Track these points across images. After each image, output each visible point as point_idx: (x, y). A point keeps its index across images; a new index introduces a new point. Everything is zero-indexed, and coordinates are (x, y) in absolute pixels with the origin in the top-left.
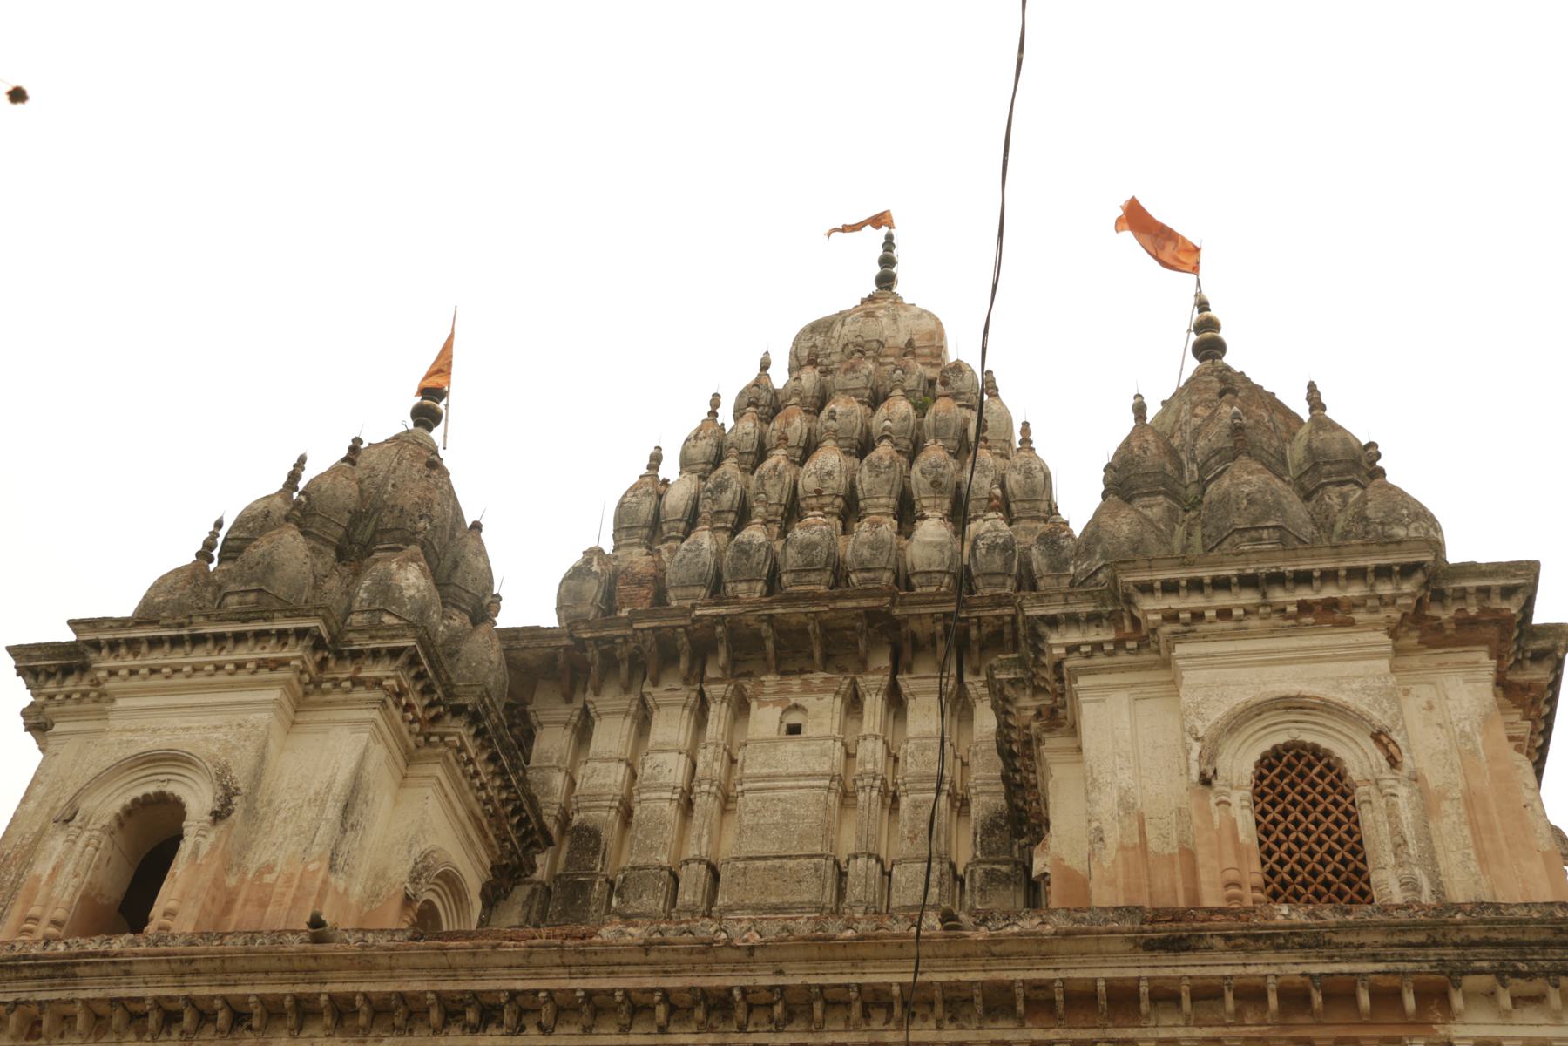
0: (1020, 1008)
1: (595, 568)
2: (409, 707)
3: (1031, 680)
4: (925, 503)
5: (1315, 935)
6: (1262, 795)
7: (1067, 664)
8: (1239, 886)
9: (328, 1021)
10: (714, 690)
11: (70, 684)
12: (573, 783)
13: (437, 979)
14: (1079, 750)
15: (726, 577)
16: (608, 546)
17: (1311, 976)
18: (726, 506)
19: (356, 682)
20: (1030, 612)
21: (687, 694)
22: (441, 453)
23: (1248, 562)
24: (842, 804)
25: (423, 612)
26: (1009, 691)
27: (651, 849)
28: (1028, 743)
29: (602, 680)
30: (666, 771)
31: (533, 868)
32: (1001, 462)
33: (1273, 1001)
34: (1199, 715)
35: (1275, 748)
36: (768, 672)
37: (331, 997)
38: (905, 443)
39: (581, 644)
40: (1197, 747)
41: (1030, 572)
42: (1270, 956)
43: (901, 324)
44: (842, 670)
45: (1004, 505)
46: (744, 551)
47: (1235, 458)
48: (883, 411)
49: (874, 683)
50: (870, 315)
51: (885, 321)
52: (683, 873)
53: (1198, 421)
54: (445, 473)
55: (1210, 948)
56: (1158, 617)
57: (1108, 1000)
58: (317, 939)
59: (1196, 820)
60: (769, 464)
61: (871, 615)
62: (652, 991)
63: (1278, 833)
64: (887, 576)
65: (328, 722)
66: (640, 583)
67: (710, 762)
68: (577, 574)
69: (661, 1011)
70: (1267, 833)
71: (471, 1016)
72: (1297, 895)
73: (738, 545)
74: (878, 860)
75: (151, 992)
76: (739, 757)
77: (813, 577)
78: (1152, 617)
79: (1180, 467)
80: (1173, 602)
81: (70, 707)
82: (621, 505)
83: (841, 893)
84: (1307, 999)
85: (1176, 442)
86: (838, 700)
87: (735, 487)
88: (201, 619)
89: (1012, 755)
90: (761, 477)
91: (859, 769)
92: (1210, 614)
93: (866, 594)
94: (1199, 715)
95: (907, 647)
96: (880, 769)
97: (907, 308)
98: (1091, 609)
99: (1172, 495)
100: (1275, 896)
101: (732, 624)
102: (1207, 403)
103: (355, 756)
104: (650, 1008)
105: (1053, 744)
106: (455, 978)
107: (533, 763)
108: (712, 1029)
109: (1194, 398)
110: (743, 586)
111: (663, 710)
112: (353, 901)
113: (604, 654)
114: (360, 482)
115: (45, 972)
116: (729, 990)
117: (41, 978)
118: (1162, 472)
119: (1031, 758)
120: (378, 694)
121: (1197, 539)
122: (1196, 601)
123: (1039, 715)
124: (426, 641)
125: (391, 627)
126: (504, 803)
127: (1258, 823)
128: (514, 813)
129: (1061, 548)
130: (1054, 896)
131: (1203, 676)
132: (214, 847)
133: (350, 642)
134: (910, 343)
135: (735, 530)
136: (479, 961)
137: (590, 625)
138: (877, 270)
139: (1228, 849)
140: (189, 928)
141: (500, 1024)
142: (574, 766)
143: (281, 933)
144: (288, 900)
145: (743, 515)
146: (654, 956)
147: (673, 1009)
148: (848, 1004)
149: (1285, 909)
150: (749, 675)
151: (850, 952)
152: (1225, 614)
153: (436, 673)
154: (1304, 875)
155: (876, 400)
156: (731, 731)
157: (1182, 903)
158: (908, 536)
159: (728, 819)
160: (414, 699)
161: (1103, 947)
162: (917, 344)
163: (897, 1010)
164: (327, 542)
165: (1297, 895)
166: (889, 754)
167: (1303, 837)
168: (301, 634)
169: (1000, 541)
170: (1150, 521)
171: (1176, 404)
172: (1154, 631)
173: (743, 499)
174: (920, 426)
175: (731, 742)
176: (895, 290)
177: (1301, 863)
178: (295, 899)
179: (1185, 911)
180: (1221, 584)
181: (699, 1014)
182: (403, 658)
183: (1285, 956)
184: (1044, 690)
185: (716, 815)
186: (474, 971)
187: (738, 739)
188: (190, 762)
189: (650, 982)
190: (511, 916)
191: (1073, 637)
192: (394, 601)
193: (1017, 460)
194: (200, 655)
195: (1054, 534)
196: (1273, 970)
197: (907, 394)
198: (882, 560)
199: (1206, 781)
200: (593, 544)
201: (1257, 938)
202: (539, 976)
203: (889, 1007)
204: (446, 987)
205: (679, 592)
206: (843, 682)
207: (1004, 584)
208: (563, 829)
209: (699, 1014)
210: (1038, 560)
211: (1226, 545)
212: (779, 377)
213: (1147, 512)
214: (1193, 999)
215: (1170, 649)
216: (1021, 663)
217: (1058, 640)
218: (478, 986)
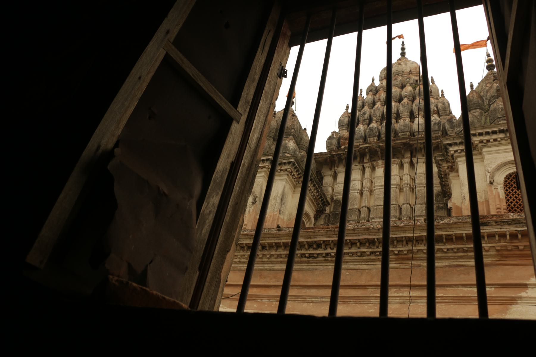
0: (444, 241)
1: (335, 136)
2: (294, 175)
3: (446, 159)
5: (519, 221)
6: (506, 186)
7: (455, 155)
8: (500, 209)
9: (283, 248)
10: (366, 165)
12: (333, 189)
13: (306, 238)
14: (459, 176)
15: (367, 136)
16: (337, 130)
17: (518, 231)
18: (366, 118)
19: (281, 170)
20: (445, 143)
21: (360, 166)
22: (295, 112)
23: (501, 126)
24: (400, 191)
25: (295, 152)
26: (440, 162)
27: (353, 204)
28: (446, 175)
29: (338, 164)
31: (326, 210)
32: (436, 101)
33: (508, 237)
34: (489, 167)
35: (510, 174)
36: (379, 159)
37: (283, 243)
38: (411, 98)
39: (333, 156)
40: (489, 174)
41: (445, 129)
42: (507, 226)
43: (408, 66)
44: (398, 158)
45: (438, 113)
46: (371, 129)
47: (498, 98)
48: (404, 90)
49: (406, 161)
50: (399, 64)
51: (403, 65)
52: (361, 210)
53: (488, 88)
54: (296, 117)
55: (492, 225)
56: (478, 142)
57: (466, 238)
58: (279, 230)
59: (489, 193)
60: (376, 106)
61: (405, 144)
62: (356, 240)
63: (511, 195)
64: (408, 133)
67: (366, 183)
68: (330, 138)
69: (358, 244)
70: (508, 195)
71: (315, 246)
72: (516, 210)
73: (370, 128)
74: (410, 205)
75: (245, 242)
76: (374, 181)
78: (476, 142)
79: (483, 101)
80: (481, 138)
82: (340, 120)
83: (401, 213)
84: (517, 236)
85: (482, 94)
86: (397, 166)
87: (368, 113)
89: (442, 178)
90: (374, 110)
91: (404, 182)
92: (492, 140)
93: (403, 139)
94: (489, 167)
95: (414, 151)
96: (409, 182)
97: (409, 61)
98: (460, 141)
99: (481, 109)
100: (510, 211)
101: (370, 148)
102: (490, 83)
103: (282, 187)
104: (356, 243)
105: (452, 175)
106: (310, 238)
107: (323, 185)
108: (370, 248)
109: (487, 82)
110: (372, 139)
112: (285, 220)
113: (338, 158)
114: (277, 121)
116: (374, 239)
118: (478, 103)
119: (447, 178)
120: (286, 173)
121: (488, 120)
122: (488, 137)
123: (448, 168)
124: (296, 160)
125: (288, 157)
126: (318, 195)
127: (505, 193)
128: (320, 198)
129: (453, 123)
130: (453, 214)
131: (490, 156)
132: (253, 210)
134: (410, 71)
135: (369, 124)
136: (315, 234)
137: (335, 151)
138: (401, 51)
139: (497, 200)
140: (250, 228)
141: (321, 248)
142: (333, 185)
143: (270, 229)
144: (271, 221)
145: (370, 120)
146: (356, 232)
147: (361, 244)
148: (402, 241)
149: (512, 214)
150: (375, 161)
151: (402, 229)
152: (495, 140)
153: (300, 167)
154: (517, 205)
155: (403, 87)
156: (371, 175)
157: (486, 214)
158: (413, 122)
159: (372, 196)
160: (295, 173)
161: (464, 226)
162: (412, 71)
163: (414, 242)
164: (271, 137)
165: (516, 210)
166: (411, 178)
167: (517, 196)
170: (475, 116)
171: (482, 84)
172: (477, 145)
173: (370, 116)
174: (414, 93)
175: (371, 177)
176: (406, 56)
177: (517, 202)
178: (272, 221)
179: (486, 216)
180: (494, 133)
181: (367, 244)
182: (291, 164)
183: (511, 226)
184: (449, 162)
185: (369, 196)
186: (315, 236)
187: (373, 177)
189: (355, 238)
190: (321, 222)
191: (456, 148)
192: (288, 150)
193: (440, 100)
195: (451, 119)
196: (508, 230)
197: (411, 85)
198: (407, 129)
199: (491, 183)
200: (333, 130)
201: (504, 222)
202: (329, 237)
203: (412, 241)
204: (309, 240)
206: (398, 161)
207: (438, 133)
208: (332, 201)
209: (367, 244)
210: (447, 126)
211: (496, 122)
212: (377, 83)
213: (475, 114)
214: (488, 237)
215: (481, 150)
216: (443, 155)
217: (452, 149)
218: (316, 240)
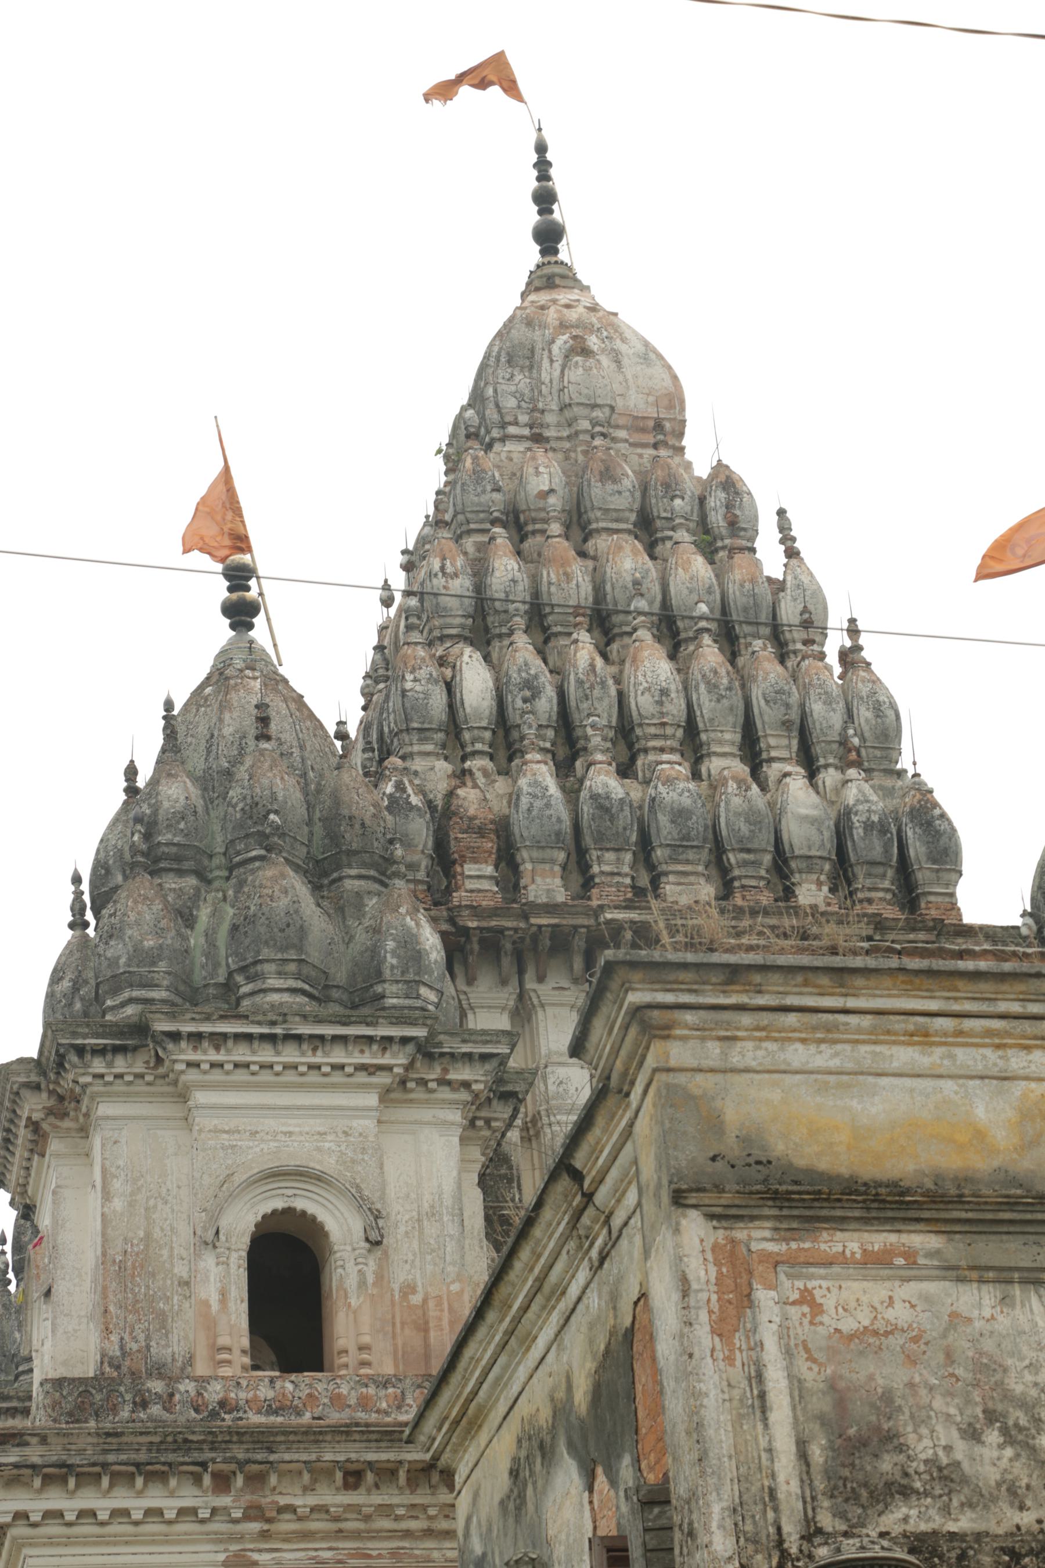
4: (772, 741)
11: (120, 1064)
30: (572, 1090)
65: (416, 1122)
66: (481, 832)
77: (691, 855)
81: (119, 1087)
88: (297, 1019)
111: (550, 1010)
115: (374, 1437)
117: (370, 1441)
133: (440, 1044)
168: (405, 1040)
169: (875, 818)
188: (319, 1179)
194: (290, 1054)
205: (535, 854)
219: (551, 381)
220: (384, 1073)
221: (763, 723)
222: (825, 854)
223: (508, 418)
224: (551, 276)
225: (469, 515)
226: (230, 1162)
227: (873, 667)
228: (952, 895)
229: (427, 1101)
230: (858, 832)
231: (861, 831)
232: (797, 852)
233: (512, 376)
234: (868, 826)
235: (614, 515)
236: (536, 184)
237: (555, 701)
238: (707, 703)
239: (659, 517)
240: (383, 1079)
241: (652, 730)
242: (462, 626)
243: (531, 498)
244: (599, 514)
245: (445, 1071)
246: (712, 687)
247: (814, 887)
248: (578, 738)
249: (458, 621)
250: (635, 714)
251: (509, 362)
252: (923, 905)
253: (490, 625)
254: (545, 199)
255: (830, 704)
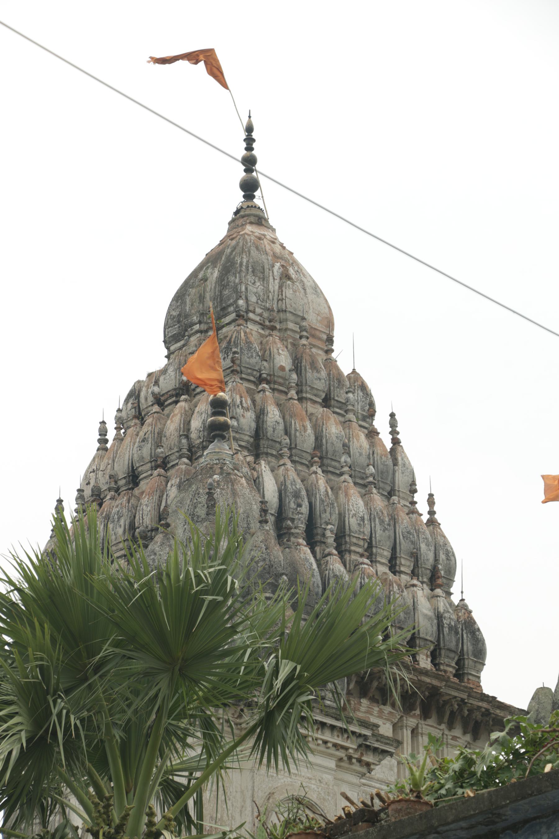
4: (403, 561)
219: (274, 292)
220: (343, 751)
221: (400, 549)
222: (432, 640)
223: (251, 308)
224: (249, 215)
225: (243, 369)
226: (270, 785)
227: (441, 526)
228: (479, 677)
229: (347, 769)
230: (446, 630)
231: (447, 629)
232: (421, 635)
233: (255, 282)
234: (450, 628)
235: (315, 392)
236: (244, 152)
237: (308, 508)
238: (379, 531)
239: (334, 399)
240: (341, 754)
241: (354, 540)
242: (248, 442)
243: (276, 368)
244: (308, 389)
245: (362, 754)
246: (382, 522)
247: (425, 657)
248: (317, 534)
249: (247, 438)
250: (347, 528)
251: (253, 272)
252: (466, 680)
253: (261, 446)
254: (249, 162)
255: (428, 546)
